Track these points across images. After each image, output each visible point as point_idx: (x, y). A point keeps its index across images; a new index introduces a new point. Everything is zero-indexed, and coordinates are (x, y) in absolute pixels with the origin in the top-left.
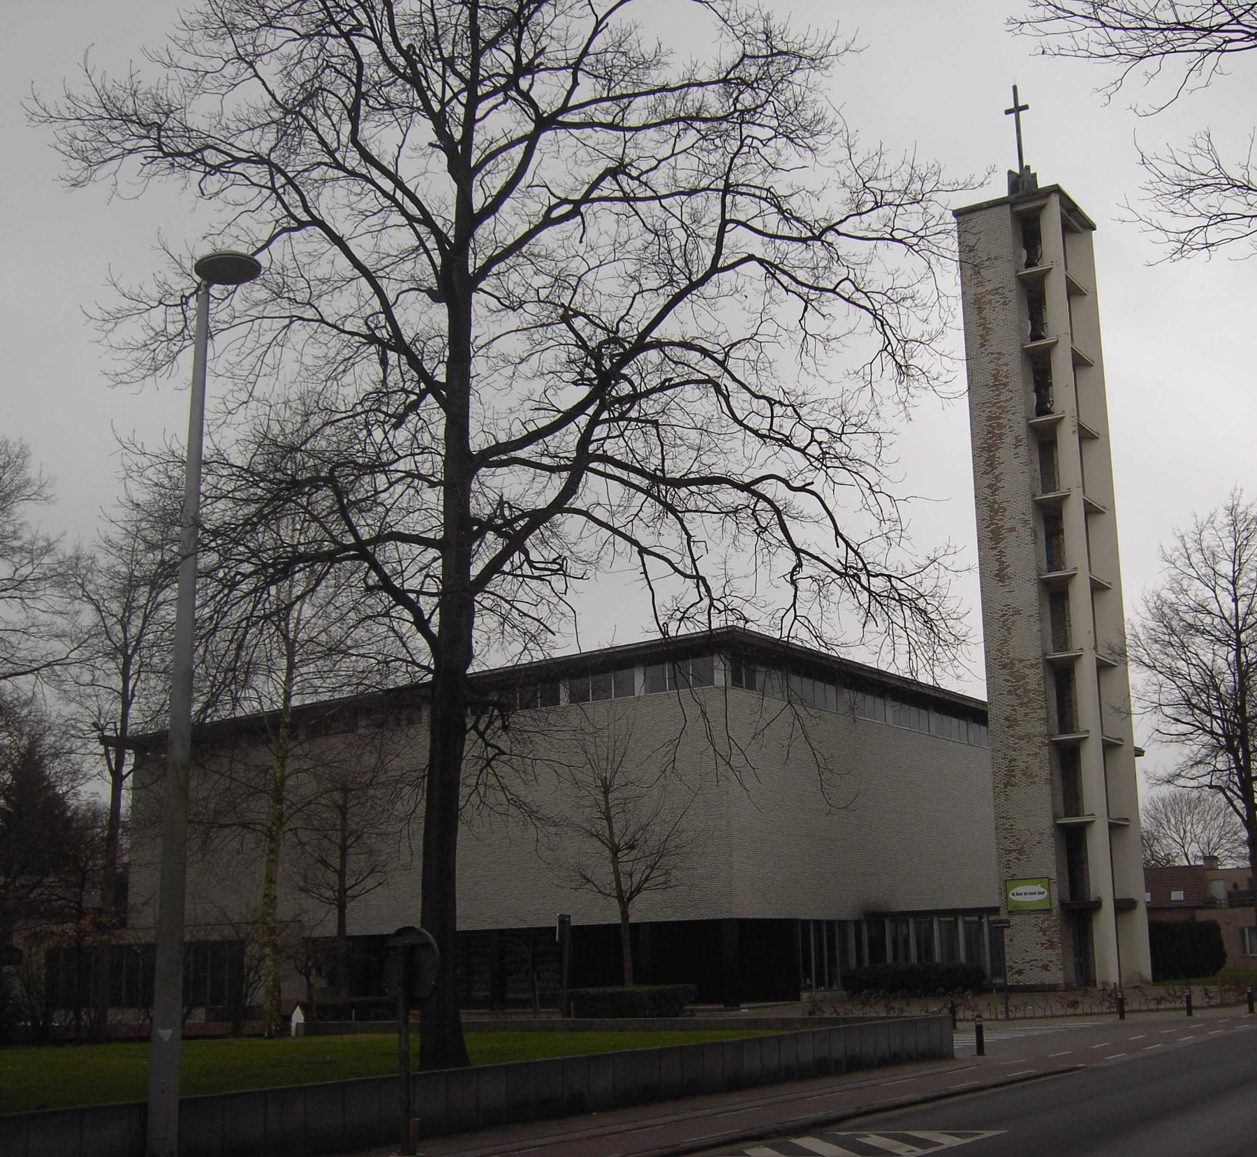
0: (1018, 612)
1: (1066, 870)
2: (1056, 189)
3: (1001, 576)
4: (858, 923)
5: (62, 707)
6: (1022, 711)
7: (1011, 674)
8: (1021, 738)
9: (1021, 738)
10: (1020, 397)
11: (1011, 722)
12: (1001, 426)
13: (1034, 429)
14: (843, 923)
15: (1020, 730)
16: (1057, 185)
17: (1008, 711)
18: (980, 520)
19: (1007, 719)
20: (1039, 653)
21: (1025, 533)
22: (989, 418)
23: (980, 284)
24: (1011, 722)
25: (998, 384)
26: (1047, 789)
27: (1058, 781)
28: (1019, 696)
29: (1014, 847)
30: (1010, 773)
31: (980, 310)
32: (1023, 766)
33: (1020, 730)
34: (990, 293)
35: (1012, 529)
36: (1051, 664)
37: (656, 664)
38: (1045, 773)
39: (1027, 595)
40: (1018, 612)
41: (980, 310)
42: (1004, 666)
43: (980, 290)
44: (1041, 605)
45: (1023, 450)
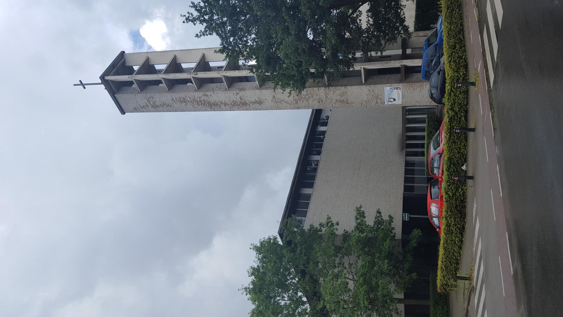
0: (274, 96)
4: (408, 154)
6: (315, 97)
7: (300, 100)
8: (327, 97)
9: (327, 97)
14: (407, 164)
15: (323, 98)
16: (100, 78)
17: (316, 102)
18: (239, 109)
19: (319, 102)
21: (242, 93)
22: (198, 105)
23: (147, 106)
25: (184, 101)
26: (349, 87)
27: (345, 80)
29: (375, 101)
32: (339, 97)
33: (323, 98)
35: (241, 99)
38: (342, 89)
40: (274, 96)
42: (297, 103)
43: (149, 106)
45: (208, 93)
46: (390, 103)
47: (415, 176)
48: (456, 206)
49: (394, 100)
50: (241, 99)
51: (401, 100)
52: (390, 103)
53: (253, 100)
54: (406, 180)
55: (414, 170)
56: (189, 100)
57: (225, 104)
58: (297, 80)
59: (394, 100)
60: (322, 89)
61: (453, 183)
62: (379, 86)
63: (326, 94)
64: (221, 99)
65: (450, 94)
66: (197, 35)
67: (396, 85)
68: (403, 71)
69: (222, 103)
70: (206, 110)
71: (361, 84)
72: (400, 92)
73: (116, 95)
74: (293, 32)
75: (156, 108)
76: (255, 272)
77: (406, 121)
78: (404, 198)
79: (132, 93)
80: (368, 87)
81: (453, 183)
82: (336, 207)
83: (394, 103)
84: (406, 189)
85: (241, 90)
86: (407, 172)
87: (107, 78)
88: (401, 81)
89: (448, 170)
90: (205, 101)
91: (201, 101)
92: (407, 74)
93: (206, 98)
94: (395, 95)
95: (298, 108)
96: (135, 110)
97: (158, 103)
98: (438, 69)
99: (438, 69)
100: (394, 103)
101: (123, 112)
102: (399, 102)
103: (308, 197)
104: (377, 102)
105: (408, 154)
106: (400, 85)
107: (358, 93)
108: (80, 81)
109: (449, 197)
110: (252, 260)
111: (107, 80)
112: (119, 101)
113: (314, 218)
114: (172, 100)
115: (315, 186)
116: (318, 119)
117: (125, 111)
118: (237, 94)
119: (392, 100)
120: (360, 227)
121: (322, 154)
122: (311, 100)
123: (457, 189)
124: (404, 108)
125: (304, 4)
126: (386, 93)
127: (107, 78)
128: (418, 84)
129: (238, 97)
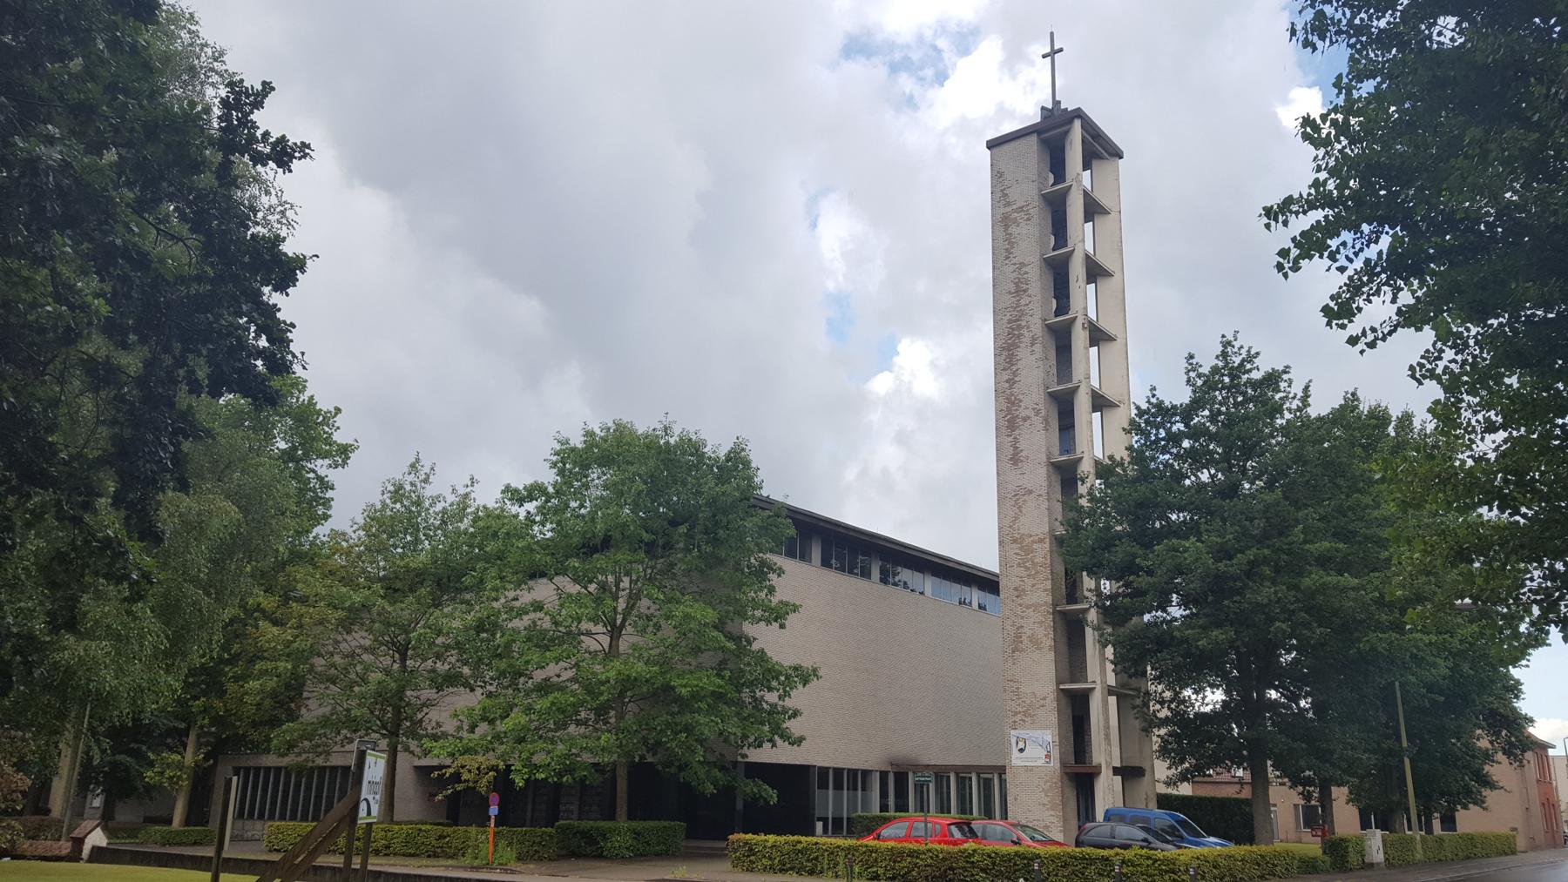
0: (1031, 492)
1: (1071, 735)
2: (1078, 114)
3: (1015, 459)
4: (884, 775)
5: (152, 601)
6: (1029, 582)
8: (1028, 607)
9: (1028, 607)
10: (1039, 307)
11: (1019, 592)
12: (1019, 327)
13: (1051, 329)
14: (866, 774)
15: (1027, 600)
16: (1079, 109)
17: (1016, 582)
18: (998, 411)
19: (1016, 589)
20: (1047, 529)
21: (1037, 421)
22: (1010, 321)
23: (1008, 204)
24: (1019, 592)
25: (1019, 290)
26: (1052, 655)
27: (1064, 649)
28: (1027, 569)
30: (1018, 637)
31: (1006, 227)
32: (1029, 633)
33: (1027, 600)
34: (1015, 211)
35: (1025, 419)
36: (1054, 396)
37: (1252, 828)
38: (1050, 642)
39: (1037, 477)
40: (1031, 492)
41: (1006, 227)
42: (1015, 541)
43: (1008, 209)
44: (1050, 485)
45: (1038, 348)
46: (1013, 741)
47: (831, 791)
48: (952, 869)
49: (1021, 750)
50: (1025, 419)
51: (1019, 763)
52: (1013, 741)
53: (1022, 445)
54: (838, 772)
55: (856, 789)
56: (1022, 302)
57: (1011, 382)
58: (1079, 550)
59: (1021, 750)
60: (1049, 599)
61: (994, 864)
62: (1053, 718)
63: (1036, 607)
64: (1023, 373)
65: (1149, 858)
66: (1191, 357)
67: (1056, 754)
68: (1081, 769)
69: (1015, 374)
70: (996, 336)
71: (1059, 683)
72: (1041, 762)
73: (1034, 138)
74: (1221, 566)
75: (1003, 223)
76: (693, 447)
77: (963, 775)
78: (808, 767)
79: (1039, 174)
80: (1052, 696)
81: (994, 864)
82: (809, 619)
83: (1015, 752)
84: (824, 771)
85: (1046, 420)
86: (853, 773)
87: (1077, 124)
88: (1063, 764)
89: (1016, 854)
90: (1019, 336)
91: (1019, 327)
92: (1080, 780)
93: (1026, 340)
94: (1034, 752)
95: (1001, 543)
96: (997, 175)
97: (1013, 230)
98: (1151, 839)
99: (1151, 839)
100: (1015, 752)
101: (992, 145)
102: (1016, 759)
103: (865, 574)
104: (1016, 713)
105: (884, 775)
106: (1055, 764)
107: (1039, 674)
108: (1061, 50)
109: (970, 855)
110: (717, 444)
111: (1071, 121)
112: (1019, 142)
113: (798, 579)
114: (1022, 264)
115: (826, 572)
116: (987, 583)
117: (995, 150)
118: (1038, 413)
119: (1021, 745)
120: (770, 674)
121: (882, 586)
122: (1021, 571)
123: (983, 870)
124: (1001, 771)
125: (1276, 592)
126: (1037, 733)
127: (1077, 124)
128: (1058, 800)
129: (1027, 413)
